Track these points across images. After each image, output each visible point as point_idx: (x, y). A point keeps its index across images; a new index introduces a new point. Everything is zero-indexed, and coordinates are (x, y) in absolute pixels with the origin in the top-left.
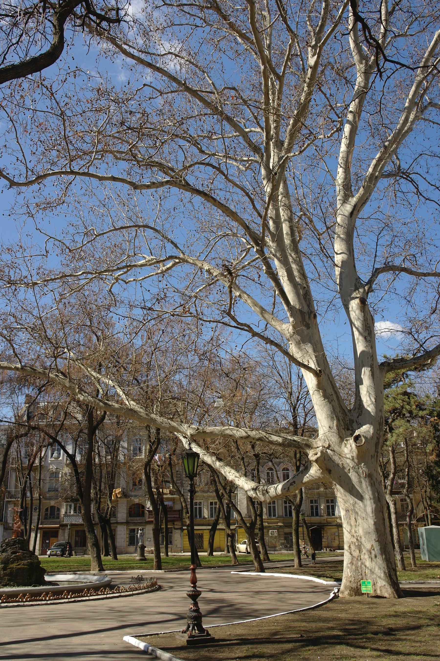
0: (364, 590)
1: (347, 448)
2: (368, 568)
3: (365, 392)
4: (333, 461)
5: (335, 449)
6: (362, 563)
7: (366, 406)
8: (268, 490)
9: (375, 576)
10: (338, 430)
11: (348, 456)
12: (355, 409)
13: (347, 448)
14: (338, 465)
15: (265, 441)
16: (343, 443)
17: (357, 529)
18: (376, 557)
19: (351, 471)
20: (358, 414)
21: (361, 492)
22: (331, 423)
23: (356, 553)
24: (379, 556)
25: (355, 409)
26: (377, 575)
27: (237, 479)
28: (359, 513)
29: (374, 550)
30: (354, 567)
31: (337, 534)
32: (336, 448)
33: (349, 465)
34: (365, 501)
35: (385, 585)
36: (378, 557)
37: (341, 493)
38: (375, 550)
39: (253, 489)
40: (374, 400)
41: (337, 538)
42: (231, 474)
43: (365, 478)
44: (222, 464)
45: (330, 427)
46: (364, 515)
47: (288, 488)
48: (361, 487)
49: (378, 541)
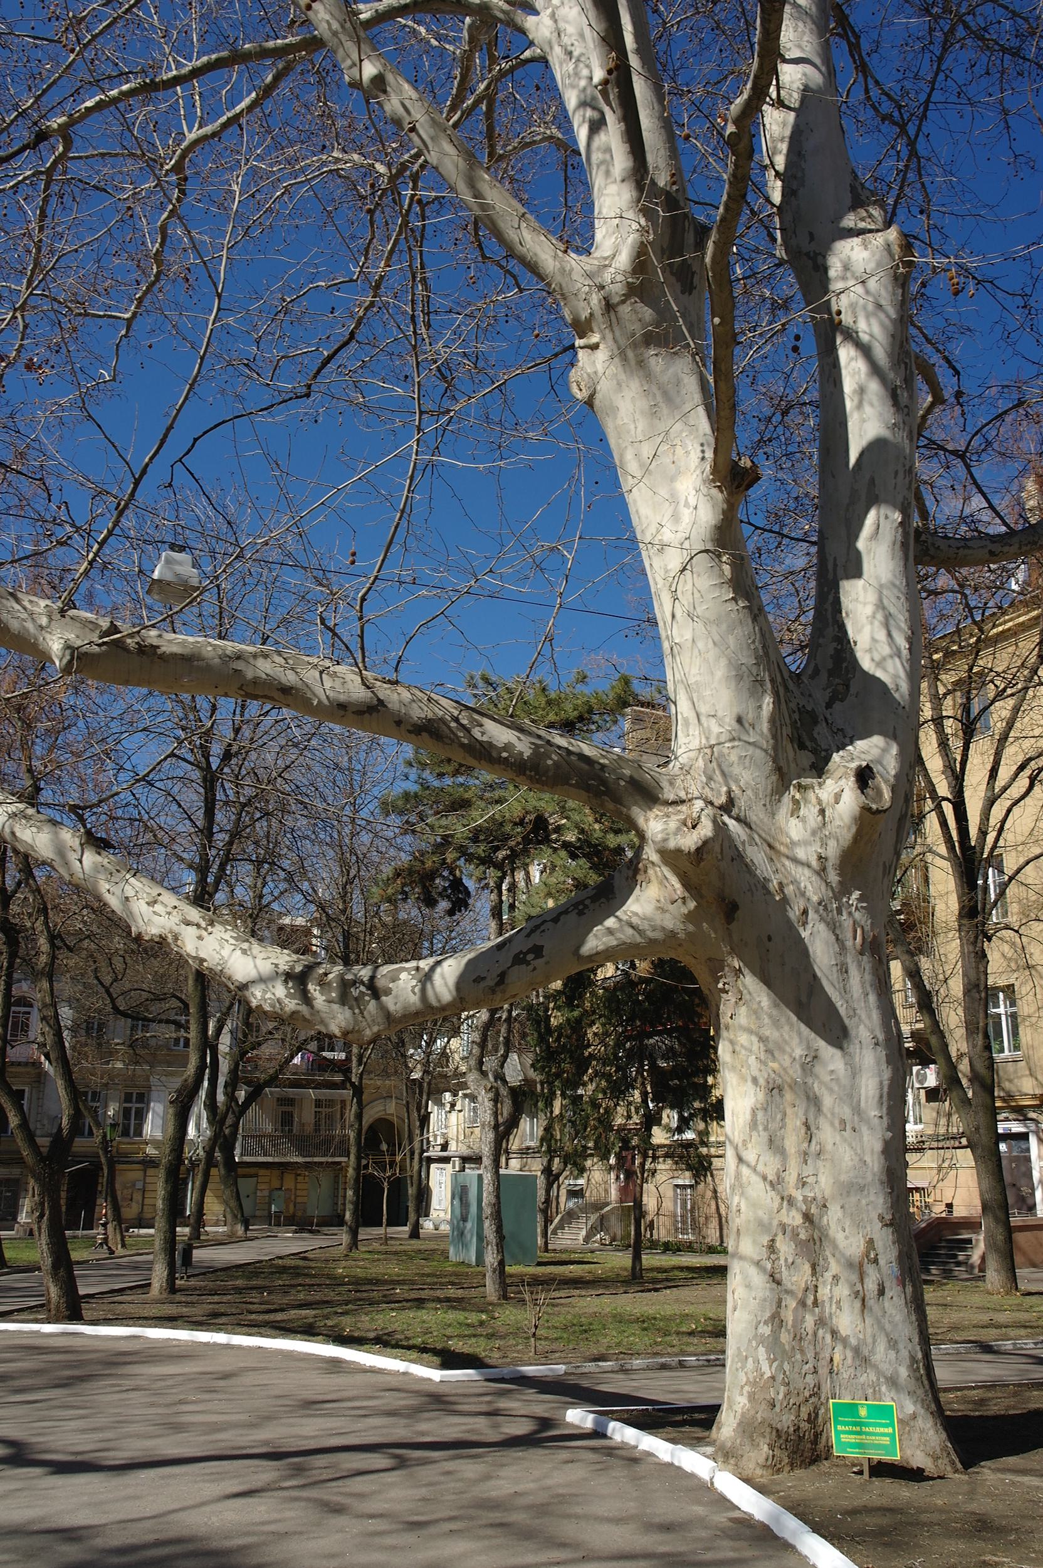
0: (843, 1440)
1: (804, 820)
2: (845, 1341)
3: (869, 610)
4: (748, 868)
5: (753, 818)
6: (821, 1322)
7: (866, 663)
8: (381, 983)
9: (873, 1377)
10: (774, 737)
11: (800, 853)
12: (816, 672)
13: (804, 820)
14: (764, 884)
15: (453, 740)
16: (786, 799)
17: (808, 1170)
18: (881, 1292)
19: (811, 914)
20: (828, 694)
21: (842, 1011)
22: (752, 704)
23: (798, 1278)
24: (893, 1291)
25: (816, 672)
26: (879, 1373)
27: (191, 931)
28: (827, 1101)
29: (876, 1261)
30: (785, 1337)
31: (139, 1185)
32: (757, 815)
33: (803, 894)
34: (853, 1048)
35: (914, 1417)
36: (889, 1293)
37: (756, 1013)
38: (882, 1262)
39: (288, 976)
40: (903, 644)
41: (137, 1196)
42: (158, 908)
43: (862, 953)
44: (105, 859)
45: (739, 720)
46: (846, 1112)
47: (502, 977)
48: (845, 991)
49: (890, 1224)
